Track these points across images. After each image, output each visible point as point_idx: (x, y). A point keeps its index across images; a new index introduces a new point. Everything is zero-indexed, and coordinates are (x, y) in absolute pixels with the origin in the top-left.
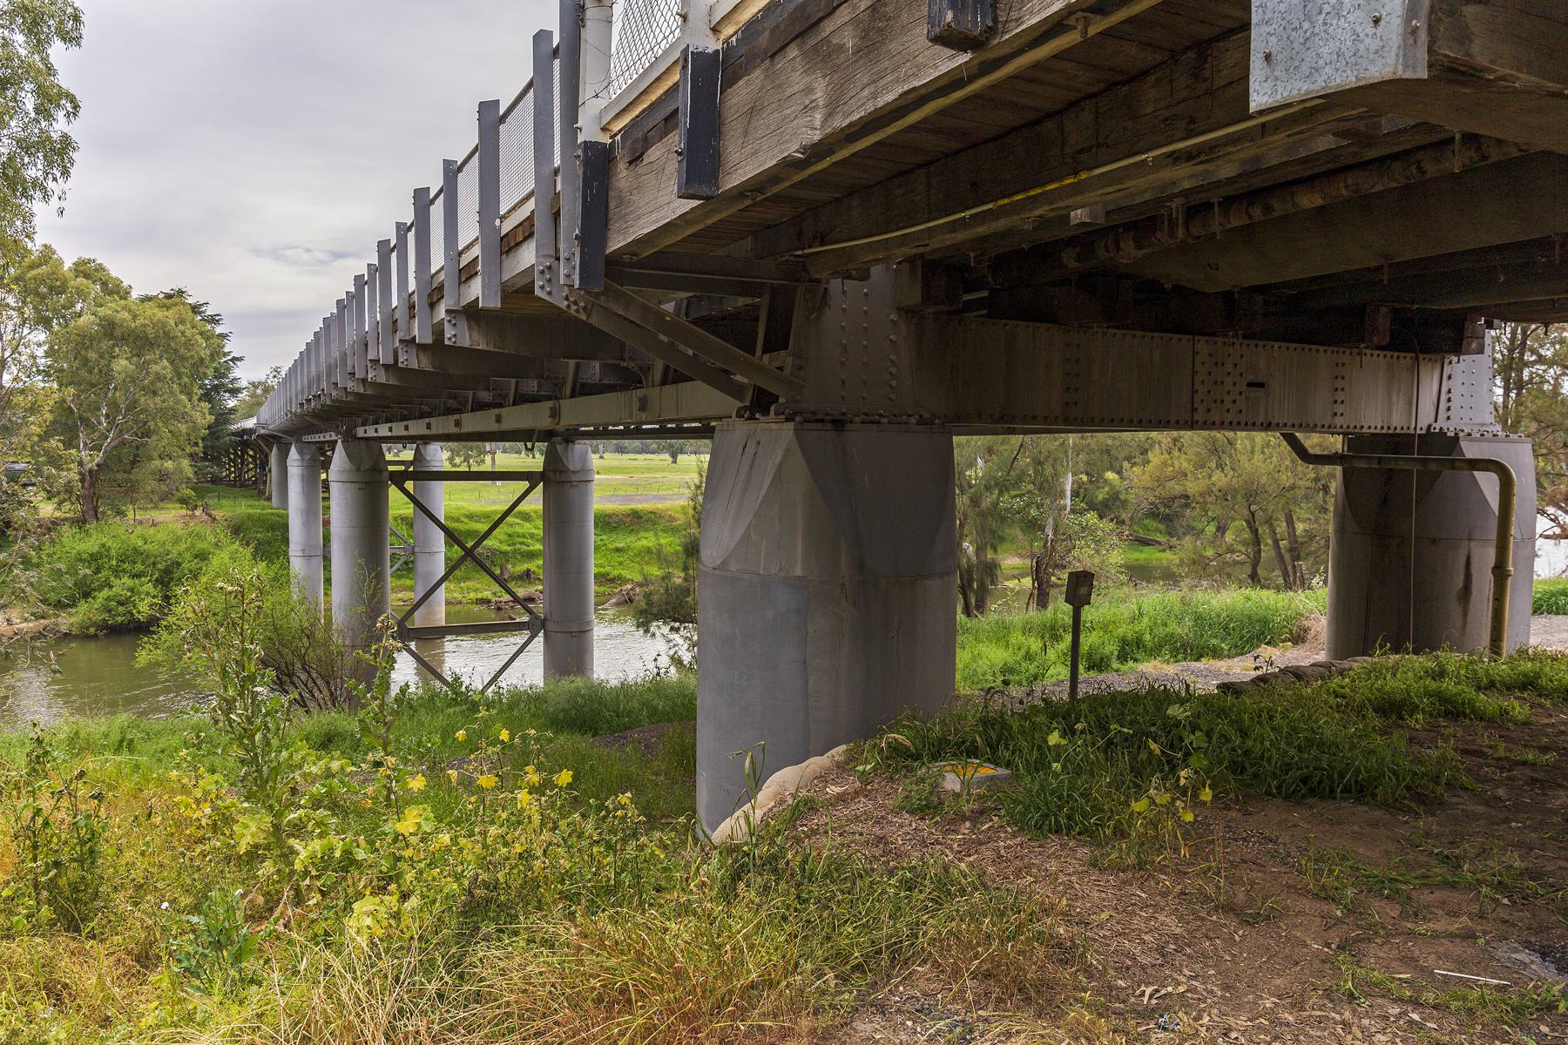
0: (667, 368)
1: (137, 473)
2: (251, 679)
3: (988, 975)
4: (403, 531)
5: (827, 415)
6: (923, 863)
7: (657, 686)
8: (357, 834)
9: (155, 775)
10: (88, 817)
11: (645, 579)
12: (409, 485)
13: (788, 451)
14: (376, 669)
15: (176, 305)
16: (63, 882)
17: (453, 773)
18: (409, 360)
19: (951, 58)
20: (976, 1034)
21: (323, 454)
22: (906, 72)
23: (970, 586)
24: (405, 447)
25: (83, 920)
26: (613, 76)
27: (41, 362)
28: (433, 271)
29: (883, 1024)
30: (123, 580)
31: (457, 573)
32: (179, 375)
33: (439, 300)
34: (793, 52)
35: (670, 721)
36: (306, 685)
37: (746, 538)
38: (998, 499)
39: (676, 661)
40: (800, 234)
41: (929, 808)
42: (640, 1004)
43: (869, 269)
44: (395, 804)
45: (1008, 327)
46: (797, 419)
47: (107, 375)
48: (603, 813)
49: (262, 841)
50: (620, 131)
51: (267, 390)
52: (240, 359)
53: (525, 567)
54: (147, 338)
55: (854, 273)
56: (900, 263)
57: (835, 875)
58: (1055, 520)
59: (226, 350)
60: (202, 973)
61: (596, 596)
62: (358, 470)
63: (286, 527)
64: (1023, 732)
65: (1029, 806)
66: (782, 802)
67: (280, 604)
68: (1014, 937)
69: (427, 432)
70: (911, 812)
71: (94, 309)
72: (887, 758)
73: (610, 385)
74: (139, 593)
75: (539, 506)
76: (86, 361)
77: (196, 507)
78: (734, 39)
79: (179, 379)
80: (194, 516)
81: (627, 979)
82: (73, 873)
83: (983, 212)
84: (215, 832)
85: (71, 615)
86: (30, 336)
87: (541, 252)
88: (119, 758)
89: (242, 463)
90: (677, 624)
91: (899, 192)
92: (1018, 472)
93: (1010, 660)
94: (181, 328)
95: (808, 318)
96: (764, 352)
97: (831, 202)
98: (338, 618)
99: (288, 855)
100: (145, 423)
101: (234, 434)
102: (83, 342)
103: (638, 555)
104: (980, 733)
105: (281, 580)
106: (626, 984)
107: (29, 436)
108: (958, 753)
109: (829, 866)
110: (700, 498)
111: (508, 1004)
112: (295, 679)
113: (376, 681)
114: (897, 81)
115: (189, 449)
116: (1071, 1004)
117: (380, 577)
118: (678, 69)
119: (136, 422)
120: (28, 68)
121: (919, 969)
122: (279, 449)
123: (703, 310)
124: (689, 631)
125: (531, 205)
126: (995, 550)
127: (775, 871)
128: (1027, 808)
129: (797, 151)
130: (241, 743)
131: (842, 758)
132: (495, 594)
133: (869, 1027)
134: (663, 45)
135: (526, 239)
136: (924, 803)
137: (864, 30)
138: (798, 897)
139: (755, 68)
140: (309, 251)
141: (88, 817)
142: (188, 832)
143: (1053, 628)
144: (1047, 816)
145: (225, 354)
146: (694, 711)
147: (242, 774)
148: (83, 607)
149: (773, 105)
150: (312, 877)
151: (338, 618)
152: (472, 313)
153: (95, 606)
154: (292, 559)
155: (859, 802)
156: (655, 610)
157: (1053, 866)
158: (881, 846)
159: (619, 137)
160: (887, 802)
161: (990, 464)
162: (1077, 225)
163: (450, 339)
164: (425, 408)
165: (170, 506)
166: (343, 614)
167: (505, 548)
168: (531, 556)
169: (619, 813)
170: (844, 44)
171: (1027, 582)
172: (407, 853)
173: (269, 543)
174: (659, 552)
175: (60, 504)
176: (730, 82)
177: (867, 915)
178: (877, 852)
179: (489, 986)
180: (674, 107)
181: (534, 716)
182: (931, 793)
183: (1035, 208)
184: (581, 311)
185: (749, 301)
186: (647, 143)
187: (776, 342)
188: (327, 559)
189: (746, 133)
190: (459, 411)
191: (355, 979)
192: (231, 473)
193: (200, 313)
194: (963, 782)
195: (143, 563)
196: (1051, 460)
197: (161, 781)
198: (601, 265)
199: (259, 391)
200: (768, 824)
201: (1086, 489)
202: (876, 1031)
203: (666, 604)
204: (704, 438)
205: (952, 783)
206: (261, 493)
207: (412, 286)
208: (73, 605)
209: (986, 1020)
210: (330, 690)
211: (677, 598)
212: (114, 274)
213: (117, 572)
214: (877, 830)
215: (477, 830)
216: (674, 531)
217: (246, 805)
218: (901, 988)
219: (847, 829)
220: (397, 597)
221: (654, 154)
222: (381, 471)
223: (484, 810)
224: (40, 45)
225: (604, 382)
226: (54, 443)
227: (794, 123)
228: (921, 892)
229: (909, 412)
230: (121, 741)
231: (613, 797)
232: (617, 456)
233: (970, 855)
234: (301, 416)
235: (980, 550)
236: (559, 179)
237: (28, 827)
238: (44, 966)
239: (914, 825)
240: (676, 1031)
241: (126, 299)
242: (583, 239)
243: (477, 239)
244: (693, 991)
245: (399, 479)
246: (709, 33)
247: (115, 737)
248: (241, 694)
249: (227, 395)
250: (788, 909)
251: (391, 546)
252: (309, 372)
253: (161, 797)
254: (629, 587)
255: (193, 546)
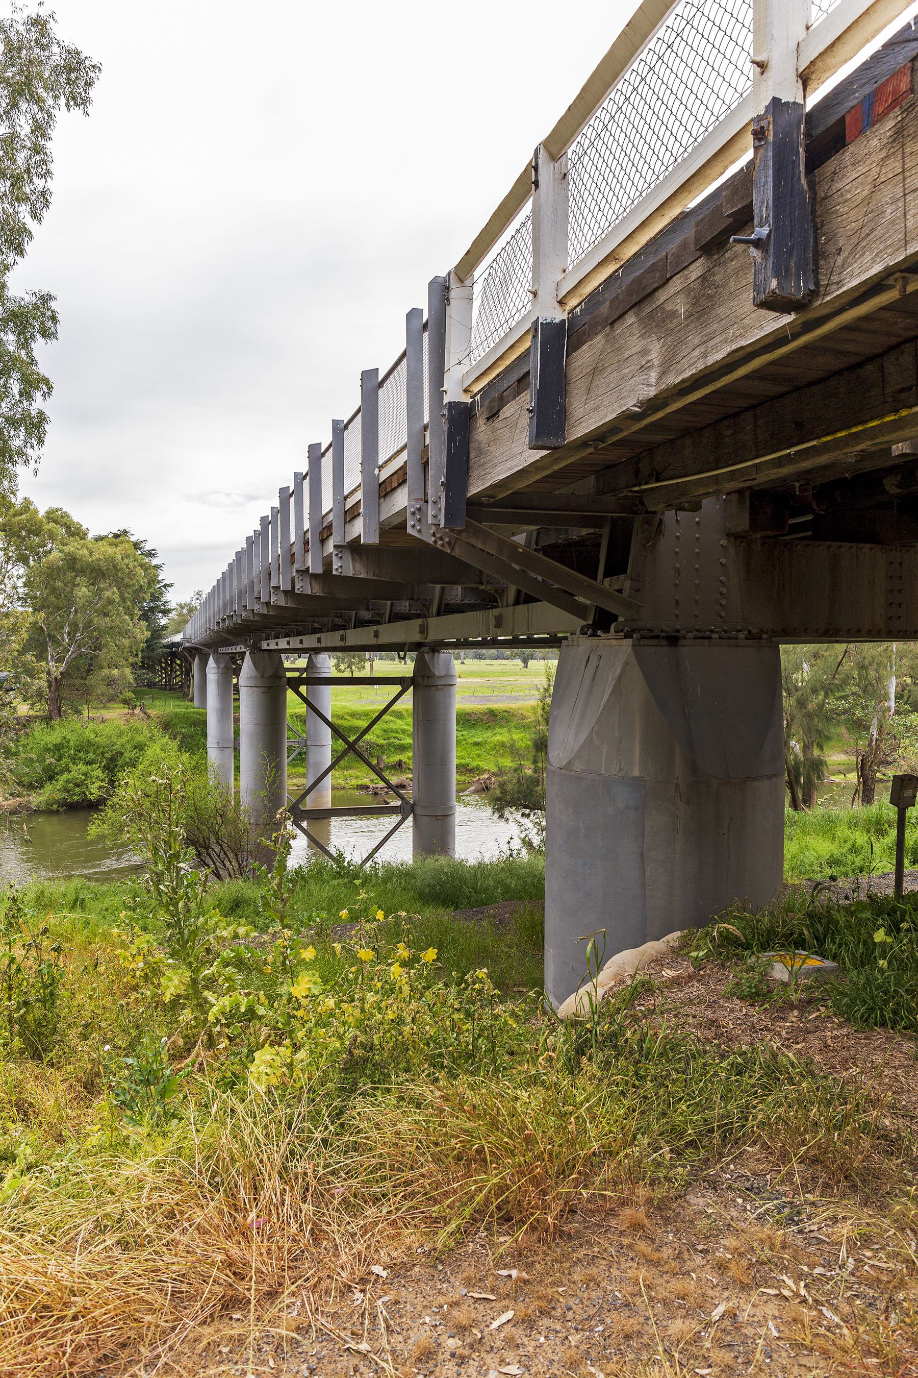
0: (519, 592)
1: (92, 680)
2: (176, 856)
3: (815, 1161)
4: (298, 727)
5: (662, 631)
6: (754, 1049)
7: (509, 866)
8: (258, 989)
9: (101, 931)
10: (50, 966)
11: (500, 770)
12: (303, 689)
13: (626, 664)
14: (274, 853)
15: (122, 543)
16: (30, 1018)
17: (337, 946)
18: (304, 587)
19: (775, 319)
20: (804, 1216)
21: (235, 663)
22: (734, 333)
23: (798, 781)
24: (300, 657)
25: (44, 1050)
26: (474, 345)
27: (20, 590)
28: (324, 513)
29: (715, 1199)
30: (79, 767)
31: (342, 763)
32: (123, 600)
33: (328, 537)
34: (631, 319)
35: (521, 898)
36: (219, 856)
37: (589, 742)
38: (824, 701)
39: (528, 844)
40: (637, 472)
41: (758, 995)
42: (494, 1165)
43: (700, 502)
44: (289, 970)
45: (832, 549)
46: (635, 636)
47: (70, 601)
48: (463, 985)
49: (183, 993)
50: (480, 391)
51: (191, 610)
52: (171, 585)
53: (397, 758)
54: (100, 569)
55: (687, 505)
56: (728, 494)
57: (671, 1055)
58: (880, 721)
59: (160, 578)
60: (134, 1106)
61: (457, 784)
62: (262, 676)
63: (204, 723)
64: (849, 927)
65: (855, 999)
66: (622, 982)
67: (200, 788)
68: (840, 1126)
69: (318, 645)
70: (742, 998)
71: (61, 547)
72: (719, 946)
73: (470, 604)
74: (91, 777)
75: (410, 706)
76: (54, 590)
77: (135, 707)
78: (578, 309)
79: (124, 602)
80: (133, 714)
81: (483, 1142)
82: (38, 1011)
83: (807, 449)
84: (146, 981)
85: (39, 794)
86: (13, 570)
87: (412, 497)
88: (73, 915)
89: (171, 670)
90: (527, 811)
91: (728, 433)
92: (843, 676)
93: (837, 852)
94: (126, 561)
95: (644, 546)
96: (605, 576)
97: (665, 443)
98: (245, 800)
99: (203, 1006)
100: (98, 639)
101: (166, 647)
102: (53, 572)
103: (493, 749)
104: (807, 926)
105: (200, 768)
106: (483, 1147)
107: (10, 652)
108: (786, 944)
109: (664, 1047)
110: (549, 700)
111: (381, 1155)
112: (210, 851)
113: (276, 864)
114: (725, 341)
115: (131, 660)
116: (896, 1195)
117: (278, 767)
118: (530, 337)
119: (90, 638)
120: (15, 360)
121: (749, 1149)
122: (200, 659)
123: (550, 539)
124: (538, 817)
125: (404, 456)
126: (822, 749)
127: (615, 1047)
128: (853, 1001)
129: (634, 406)
130: (168, 909)
131: (677, 944)
132: (372, 781)
133: (701, 1201)
134: (516, 317)
135: (400, 485)
136: (754, 990)
137: (695, 297)
138: (636, 1074)
139: (596, 334)
140: (228, 495)
141: (50, 966)
142: (125, 980)
143: (878, 823)
144: (872, 1009)
145: (159, 582)
146: (543, 889)
147: (168, 935)
148: (48, 788)
149: (613, 366)
150: (222, 1025)
151: (245, 800)
152: (354, 548)
153: (58, 787)
154: (209, 750)
155: (693, 986)
156: (508, 798)
157: (878, 1059)
158: (713, 1029)
159: (478, 397)
160: (718, 987)
161: (816, 668)
162: (898, 455)
163: (337, 570)
164: (316, 625)
165: (116, 706)
166: (248, 798)
167: (381, 741)
168: (402, 748)
169: (477, 986)
170: (677, 310)
171: (853, 777)
172: (300, 1013)
173: (191, 736)
174: (512, 746)
175: (33, 704)
176: (574, 347)
177: (700, 1094)
178: (710, 1034)
179: (365, 1138)
180: (526, 370)
181: (404, 889)
182: (760, 982)
183: (857, 444)
184: (446, 545)
185: (591, 531)
186: (502, 402)
187: (616, 567)
188: (237, 750)
189: (589, 391)
190: (344, 628)
191: (255, 1124)
192: (162, 678)
193: (140, 549)
194: (790, 973)
195: (94, 752)
196: (875, 665)
197: (105, 936)
198: (463, 507)
199: (185, 611)
200: (609, 1002)
201: (910, 691)
202: (708, 1205)
203: (519, 792)
204: (551, 647)
205: (780, 972)
206: (186, 695)
207: (307, 525)
208: (42, 787)
209: (813, 1204)
210: (238, 861)
211: (528, 787)
212: (76, 519)
213: (74, 760)
214: (709, 1013)
215: (356, 996)
216: (525, 727)
217: (170, 961)
218: (732, 1167)
219: (682, 1011)
220: (293, 782)
221: (508, 411)
222: (280, 678)
223: (363, 979)
224: (25, 345)
225: (465, 602)
226: (29, 657)
227: (632, 381)
228: (751, 1077)
229: (739, 628)
230: (76, 901)
231: (472, 972)
232: (476, 661)
233: (797, 1043)
234: (218, 632)
235: (806, 748)
236: (428, 434)
237: (5, 973)
238: (15, 1087)
239: (744, 1011)
240: (526, 1192)
241: (84, 539)
242: (447, 485)
243: (360, 485)
244: (539, 1157)
245: (294, 684)
246: (557, 305)
247: (71, 897)
248: (168, 869)
249: (160, 615)
250: (627, 1085)
251: (288, 740)
252: (224, 597)
253: (105, 950)
254: (486, 776)
255: (133, 739)
